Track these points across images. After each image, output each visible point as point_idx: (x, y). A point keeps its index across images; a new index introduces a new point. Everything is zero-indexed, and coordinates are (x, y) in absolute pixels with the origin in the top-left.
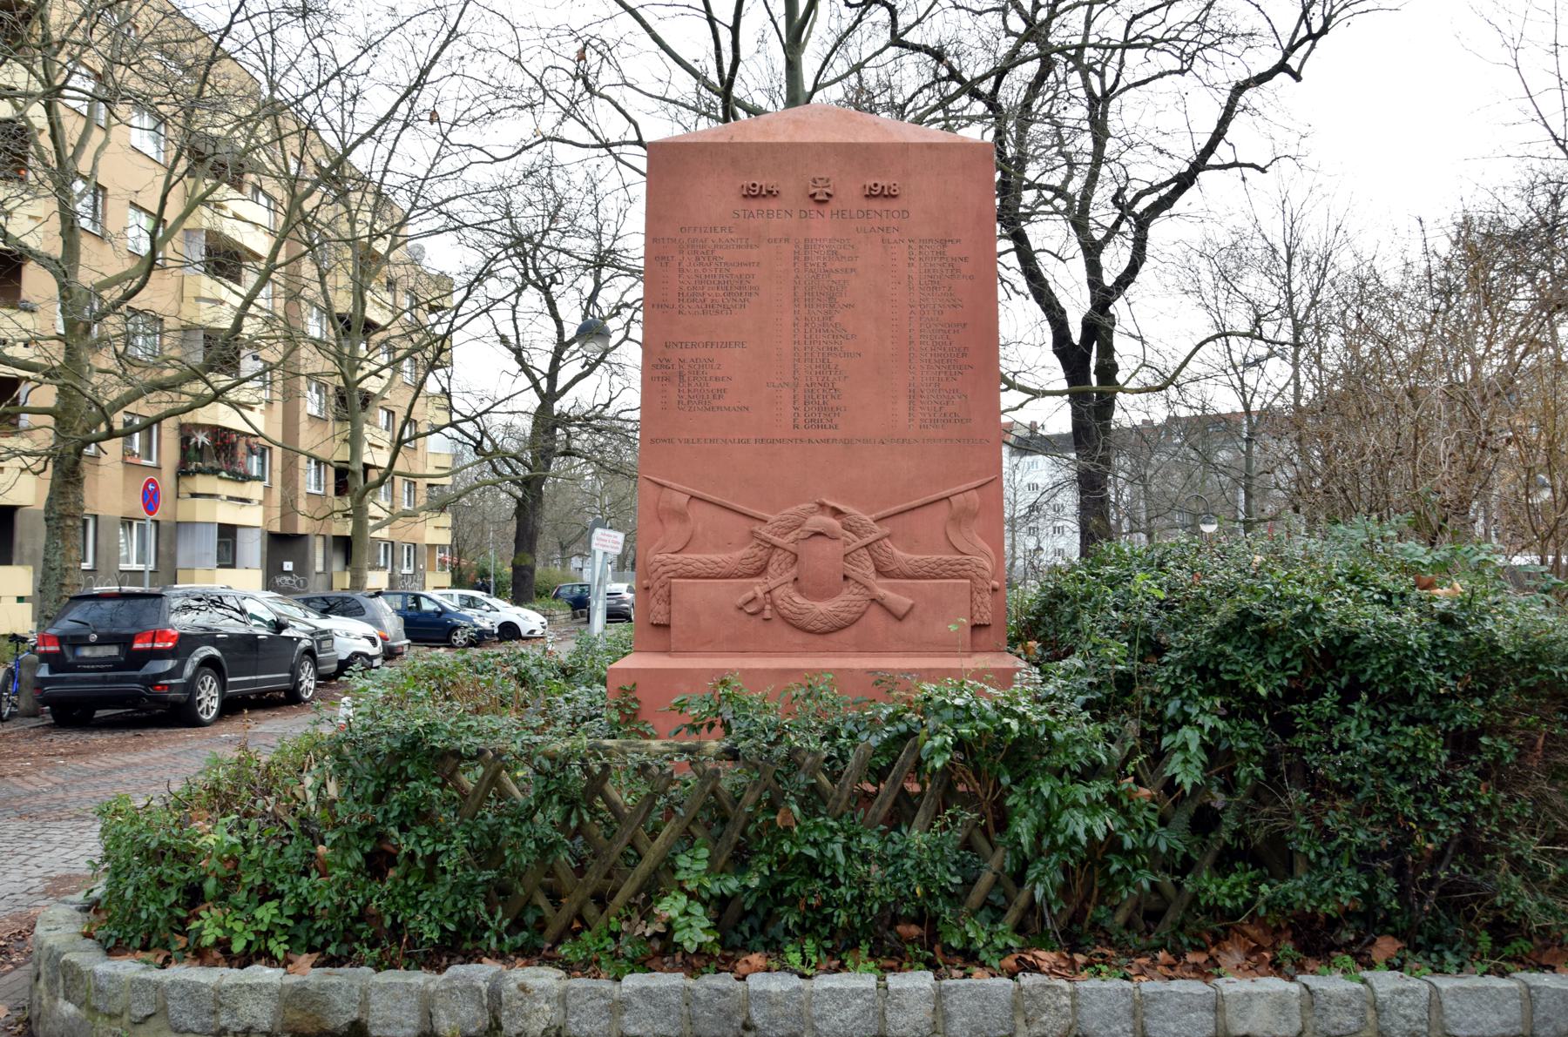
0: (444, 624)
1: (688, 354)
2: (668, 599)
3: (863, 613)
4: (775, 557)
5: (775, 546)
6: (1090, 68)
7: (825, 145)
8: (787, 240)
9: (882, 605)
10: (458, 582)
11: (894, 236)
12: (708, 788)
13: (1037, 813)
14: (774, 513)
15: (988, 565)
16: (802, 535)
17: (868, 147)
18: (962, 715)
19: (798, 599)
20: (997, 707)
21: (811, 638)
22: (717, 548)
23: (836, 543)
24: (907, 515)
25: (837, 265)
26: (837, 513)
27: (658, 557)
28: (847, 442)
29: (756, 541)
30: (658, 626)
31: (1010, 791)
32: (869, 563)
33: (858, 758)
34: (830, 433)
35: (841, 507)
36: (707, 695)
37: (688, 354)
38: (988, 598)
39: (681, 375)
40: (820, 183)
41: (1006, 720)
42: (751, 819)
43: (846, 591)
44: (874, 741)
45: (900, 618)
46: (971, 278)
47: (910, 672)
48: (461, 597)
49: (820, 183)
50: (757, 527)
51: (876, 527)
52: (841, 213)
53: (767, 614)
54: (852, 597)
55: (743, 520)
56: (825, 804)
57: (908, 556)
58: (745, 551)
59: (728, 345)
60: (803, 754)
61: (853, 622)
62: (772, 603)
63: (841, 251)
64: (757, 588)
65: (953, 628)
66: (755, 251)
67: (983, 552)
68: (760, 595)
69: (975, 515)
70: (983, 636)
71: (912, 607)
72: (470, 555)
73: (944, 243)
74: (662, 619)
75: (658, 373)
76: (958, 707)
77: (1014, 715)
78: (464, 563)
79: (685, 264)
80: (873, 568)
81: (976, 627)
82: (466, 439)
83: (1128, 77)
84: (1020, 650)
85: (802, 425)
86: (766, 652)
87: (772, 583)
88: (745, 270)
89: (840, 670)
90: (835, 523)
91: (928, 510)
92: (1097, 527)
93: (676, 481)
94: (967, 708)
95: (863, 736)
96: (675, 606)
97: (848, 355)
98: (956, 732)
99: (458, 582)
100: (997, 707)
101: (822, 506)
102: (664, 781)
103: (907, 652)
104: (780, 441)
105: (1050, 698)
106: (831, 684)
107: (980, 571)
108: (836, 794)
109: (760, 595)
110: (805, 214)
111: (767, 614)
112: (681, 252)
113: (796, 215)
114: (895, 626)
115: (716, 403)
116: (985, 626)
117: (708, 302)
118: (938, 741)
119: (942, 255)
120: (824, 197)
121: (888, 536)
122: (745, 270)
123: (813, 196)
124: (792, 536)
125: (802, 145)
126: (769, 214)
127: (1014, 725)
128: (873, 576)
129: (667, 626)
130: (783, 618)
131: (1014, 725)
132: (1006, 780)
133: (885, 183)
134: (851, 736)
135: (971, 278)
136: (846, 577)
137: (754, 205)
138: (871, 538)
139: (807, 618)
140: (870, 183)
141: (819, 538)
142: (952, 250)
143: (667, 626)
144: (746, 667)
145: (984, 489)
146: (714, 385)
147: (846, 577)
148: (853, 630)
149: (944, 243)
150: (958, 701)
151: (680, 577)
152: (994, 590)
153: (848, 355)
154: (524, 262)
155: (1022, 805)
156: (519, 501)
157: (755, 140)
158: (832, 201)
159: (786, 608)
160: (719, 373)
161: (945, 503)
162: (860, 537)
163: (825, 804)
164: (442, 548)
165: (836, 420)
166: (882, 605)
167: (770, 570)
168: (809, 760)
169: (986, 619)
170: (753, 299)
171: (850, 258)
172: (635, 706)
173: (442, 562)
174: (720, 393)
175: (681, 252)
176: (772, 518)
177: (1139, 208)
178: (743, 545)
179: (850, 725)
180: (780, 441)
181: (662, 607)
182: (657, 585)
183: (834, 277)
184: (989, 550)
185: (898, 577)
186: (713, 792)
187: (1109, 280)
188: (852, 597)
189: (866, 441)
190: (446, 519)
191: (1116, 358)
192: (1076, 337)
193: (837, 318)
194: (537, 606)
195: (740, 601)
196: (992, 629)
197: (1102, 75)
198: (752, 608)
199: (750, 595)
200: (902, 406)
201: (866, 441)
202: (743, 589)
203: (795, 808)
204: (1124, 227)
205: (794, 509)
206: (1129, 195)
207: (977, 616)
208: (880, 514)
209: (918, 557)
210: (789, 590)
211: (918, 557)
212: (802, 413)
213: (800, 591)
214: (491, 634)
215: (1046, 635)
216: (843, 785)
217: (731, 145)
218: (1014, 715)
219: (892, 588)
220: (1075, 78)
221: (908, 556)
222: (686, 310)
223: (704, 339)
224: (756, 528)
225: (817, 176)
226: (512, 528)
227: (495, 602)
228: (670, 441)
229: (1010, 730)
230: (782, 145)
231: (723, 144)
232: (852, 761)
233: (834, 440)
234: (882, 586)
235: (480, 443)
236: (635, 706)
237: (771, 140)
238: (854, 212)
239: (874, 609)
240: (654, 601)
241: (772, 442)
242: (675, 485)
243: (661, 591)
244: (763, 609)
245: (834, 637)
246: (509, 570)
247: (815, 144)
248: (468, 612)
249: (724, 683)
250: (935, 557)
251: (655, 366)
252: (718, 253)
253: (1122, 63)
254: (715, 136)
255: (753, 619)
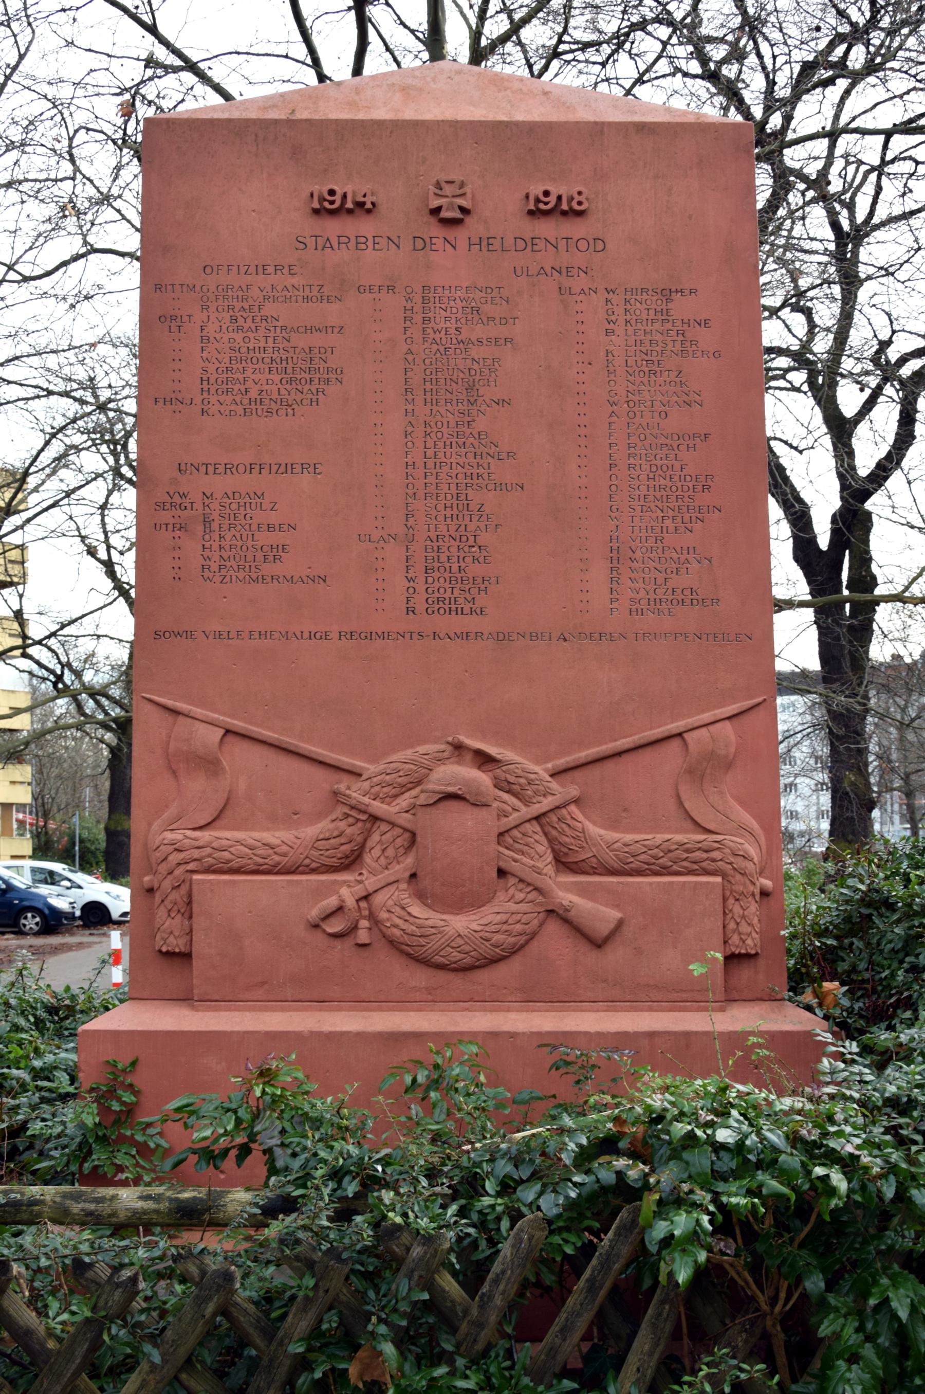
0: (10, 905)
1: (220, 484)
2: (188, 908)
3: (533, 936)
4: (376, 837)
5: (375, 819)
6: (838, 197)
7: (456, 126)
8: (391, 288)
9: (566, 921)
10: (43, 849)
11: (580, 282)
12: (210, 1308)
13: (881, 1352)
14: (374, 760)
15: (752, 851)
16: (423, 799)
17: (531, 128)
18: (728, 1163)
19: (416, 910)
20: (794, 1139)
21: (442, 977)
22: (274, 820)
23: (483, 812)
24: (610, 767)
25: (479, 331)
26: (484, 760)
27: (169, 836)
28: (502, 638)
29: (341, 810)
30: (169, 955)
31: (822, 1303)
32: (543, 847)
33: (516, 1246)
34: (471, 623)
35: (492, 750)
36: (236, 1096)
37: (220, 484)
38: (753, 907)
39: (207, 521)
40: (448, 190)
41: (819, 1171)
42: (303, 1364)
43: (501, 895)
44: (550, 1205)
45: (598, 944)
46: (716, 354)
47: (622, 1040)
48: (34, 870)
49: (448, 190)
50: (343, 784)
51: (554, 785)
52: (485, 243)
53: (363, 936)
54: (512, 907)
55: (320, 774)
56: (454, 1330)
57: (611, 835)
58: (323, 826)
59: (289, 468)
60: (405, 1238)
61: (515, 951)
62: (372, 916)
63: (487, 308)
64: (344, 891)
65: (697, 969)
66: (335, 307)
67: (743, 829)
68: (350, 902)
69: (728, 765)
70: (744, 974)
71: (620, 924)
72: (59, 817)
73: (667, 294)
74: (177, 944)
75: (166, 517)
76: (719, 1148)
77: (832, 1158)
78: (52, 825)
79: (211, 328)
80: (549, 857)
81: (731, 959)
82: (45, 674)
83: (881, 214)
84: (808, 997)
85: (421, 607)
86: (360, 1002)
87: (371, 883)
88: (317, 340)
89: (494, 1035)
90: (482, 779)
91: (647, 756)
92: (853, 784)
93: (201, 704)
94: (740, 1148)
95: (528, 1194)
96: (199, 922)
97: (501, 487)
98: (716, 1200)
99: (43, 849)
100: (794, 1139)
101: (458, 747)
102: (117, 1295)
103: (612, 1003)
104: (383, 636)
105: (893, 1103)
106: (475, 1065)
107: (739, 863)
108: (474, 1312)
109: (350, 902)
110: (422, 244)
111: (363, 936)
112: (205, 308)
113: (406, 245)
114: (590, 957)
115: (268, 569)
116: (748, 956)
117: (253, 394)
118: (681, 1223)
119: (665, 315)
120: (458, 215)
121: (576, 801)
122: (317, 340)
123: (436, 211)
124: (405, 801)
125: (416, 124)
126: (360, 242)
127: (838, 1180)
128: (550, 870)
129: (185, 957)
130: (392, 943)
131: (838, 1180)
132: (815, 1283)
133: (563, 190)
134: (507, 1187)
135: (716, 354)
136: (502, 873)
137: (333, 227)
138: (546, 804)
139: (433, 944)
140: (537, 190)
141: (454, 805)
142: (681, 308)
143: (185, 957)
144: (327, 1028)
145: (745, 719)
146: (265, 538)
147: (502, 873)
148: (515, 965)
149: (667, 294)
150: (723, 1135)
151: (208, 870)
152: (764, 894)
153: (501, 487)
154: (114, 453)
155: (850, 1336)
156: (112, 750)
157: (333, 116)
158: (469, 220)
159: (393, 921)
160: (274, 518)
161: (676, 744)
162: (527, 802)
163: (454, 1330)
164: (21, 807)
165: (481, 600)
166: (566, 921)
167: (368, 859)
168: (417, 1251)
169: (751, 945)
170: (332, 389)
171: (504, 321)
172: (128, 1098)
173: (21, 823)
174: (276, 553)
175: (205, 308)
176: (371, 768)
177: (906, 371)
178: (319, 816)
179: (504, 1167)
180: (383, 636)
181: (176, 923)
182: (167, 884)
183: (474, 352)
184: (754, 825)
185: (594, 872)
186: (224, 1311)
187: (865, 465)
188: (512, 907)
189: (535, 636)
190: (25, 772)
191: (874, 568)
192: (824, 542)
193: (481, 424)
194: (123, 880)
195: (314, 913)
196: (761, 963)
197: (851, 207)
198: (334, 926)
199: (332, 902)
200: (599, 573)
201: (535, 636)
202: (320, 892)
203: (388, 1349)
204: (889, 390)
205: (408, 754)
206: (893, 354)
207: (735, 939)
208: (562, 762)
209: (629, 837)
210: (402, 894)
211: (629, 837)
212: (421, 586)
213: (421, 896)
214: (71, 917)
215: (854, 969)
216: (490, 1297)
217: (291, 123)
218: (832, 1158)
219: (582, 891)
220: (818, 213)
221: (611, 835)
222: (214, 409)
223: (246, 457)
224: (342, 787)
225: (443, 177)
226: (106, 785)
227: (80, 877)
228: (189, 634)
229: (832, 1191)
230: (380, 124)
231: (276, 122)
232: (506, 1248)
233: (479, 635)
234: (566, 888)
235: (60, 678)
236: (128, 1098)
237: (361, 116)
238: (509, 242)
239: (553, 928)
240: (162, 913)
241: (370, 636)
242: (198, 711)
243: (175, 895)
244: (355, 928)
245: (483, 976)
246: (102, 836)
247: (438, 123)
248: (44, 890)
249: (266, 1075)
250: (660, 838)
251: (161, 506)
252: (270, 309)
253: (879, 189)
254: (265, 109)
255: (338, 944)
